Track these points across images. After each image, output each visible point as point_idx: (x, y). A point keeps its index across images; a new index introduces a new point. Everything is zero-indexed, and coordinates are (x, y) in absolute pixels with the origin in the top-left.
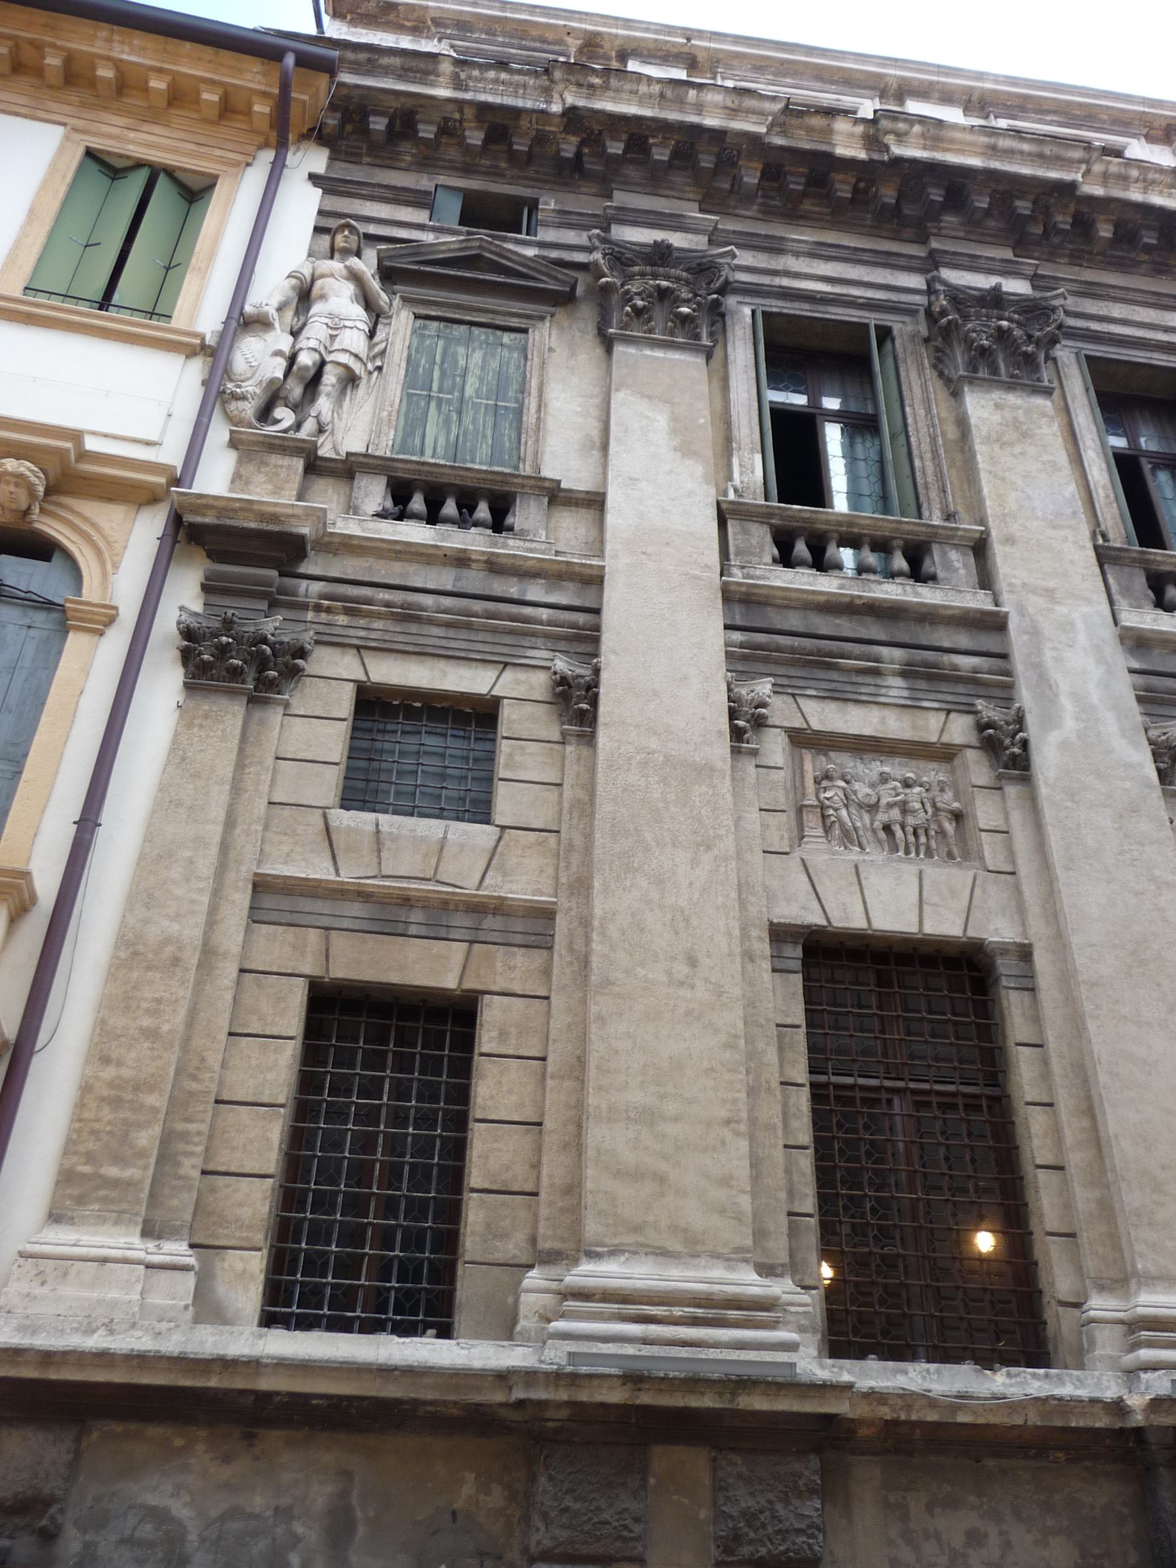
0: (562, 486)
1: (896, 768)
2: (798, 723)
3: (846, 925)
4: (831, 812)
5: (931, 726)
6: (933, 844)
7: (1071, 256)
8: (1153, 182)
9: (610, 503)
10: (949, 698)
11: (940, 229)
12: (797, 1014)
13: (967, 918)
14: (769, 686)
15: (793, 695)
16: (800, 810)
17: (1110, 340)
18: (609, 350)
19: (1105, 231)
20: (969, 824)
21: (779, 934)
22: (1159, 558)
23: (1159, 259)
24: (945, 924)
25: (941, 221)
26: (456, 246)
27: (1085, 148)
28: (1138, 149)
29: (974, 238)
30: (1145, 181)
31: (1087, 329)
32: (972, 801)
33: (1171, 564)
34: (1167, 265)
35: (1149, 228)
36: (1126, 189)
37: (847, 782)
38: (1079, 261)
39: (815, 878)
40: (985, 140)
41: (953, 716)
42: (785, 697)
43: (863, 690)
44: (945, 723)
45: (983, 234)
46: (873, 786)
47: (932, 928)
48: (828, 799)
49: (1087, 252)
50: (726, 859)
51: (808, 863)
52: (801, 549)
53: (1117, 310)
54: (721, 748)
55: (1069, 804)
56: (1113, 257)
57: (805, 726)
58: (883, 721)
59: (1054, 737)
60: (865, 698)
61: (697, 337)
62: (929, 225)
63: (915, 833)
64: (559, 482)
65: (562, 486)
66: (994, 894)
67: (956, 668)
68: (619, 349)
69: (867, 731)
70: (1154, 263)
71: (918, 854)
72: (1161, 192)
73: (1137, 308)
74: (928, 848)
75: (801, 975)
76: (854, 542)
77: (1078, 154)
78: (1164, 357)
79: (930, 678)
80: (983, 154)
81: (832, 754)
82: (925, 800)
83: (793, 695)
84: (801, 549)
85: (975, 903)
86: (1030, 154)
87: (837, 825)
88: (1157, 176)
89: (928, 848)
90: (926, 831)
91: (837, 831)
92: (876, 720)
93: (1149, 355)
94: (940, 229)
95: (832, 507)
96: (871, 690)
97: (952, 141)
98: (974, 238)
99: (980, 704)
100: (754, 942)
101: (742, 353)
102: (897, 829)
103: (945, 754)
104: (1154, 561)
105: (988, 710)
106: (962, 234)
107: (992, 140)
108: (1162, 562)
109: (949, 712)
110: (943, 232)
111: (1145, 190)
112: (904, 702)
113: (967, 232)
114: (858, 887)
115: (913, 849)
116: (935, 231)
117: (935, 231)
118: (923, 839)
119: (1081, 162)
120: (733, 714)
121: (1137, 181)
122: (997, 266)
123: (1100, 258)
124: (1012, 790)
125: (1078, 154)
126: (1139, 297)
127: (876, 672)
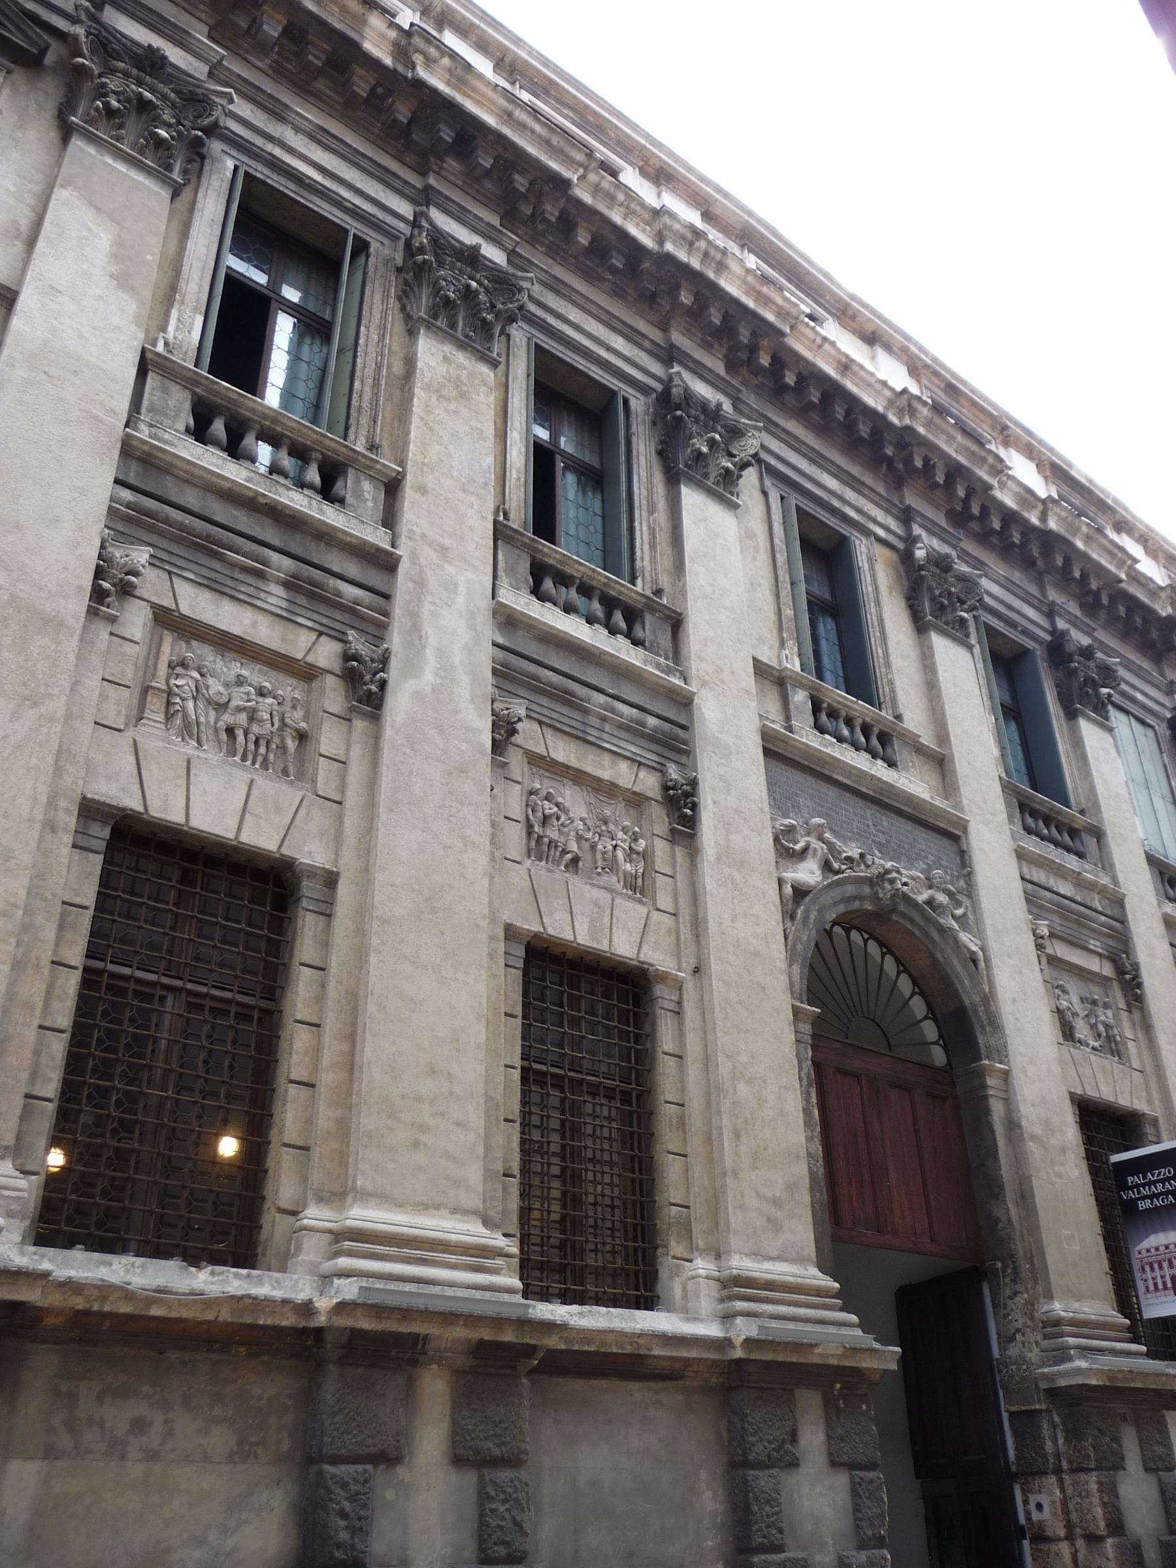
1: (255, 674)
2: (167, 602)
3: (163, 816)
4: (178, 700)
5: (300, 643)
6: (271, 757)
7: (549, 248)
8: (634, 212)
10: (325, 621)
13: (285, 836)
14: (146, 556)
15: (170, 573)
16: (146, 690)
20: (310, 746)
22: (546, 550)
24: (262, 836)
30: (627, 208)
31: (544, 321)
32: (319, 726)
37: (202, 675)
39: (142, 763)
41: (323, 639)
42: (161, 572)
43: (242, 589)
44: (314, 644)
45: (478, 191)
46: (227, 685)
47: (247, 838)
48: (177, 686)
50: (51, 720)
51: (140, 746)
54: (79, 604)
55: (408, 751)
57: (173, 607)
58: (254, 624)
59: (411, 685)
60: (242, 597)
62: (432, 159)
63: (257, 743)
66: (317, 818)
67: (339, 594)
69: (236, 630)
71: (254, 763)
72: (638, 224)
74: (266, 759)
79: (312, 596)
81: (194, 643)
82: (275, 713)
83: (170, 573)
85: (297, 822)
86: (539, 136)
87: (180, 715)
88: (638, 208)
89: (266, 759)
90: (268, 743)
91: (178, 721)
92: (247, 622)
94: (441, 168)
96: (251, 590)
99: (352, 635)
100: (61, 813)
102: (240, 734)
103: (306, 673)
104: (541, 551)
105: (358, 643)
106: (459, 183)
109: (321, 634)
110: (443, 173)
112: (279, 612)
113: (465, 183)
114: (185, 782)
115: (250, 757)
117: (436, 168)
118: (262, 750)
119: (581, 165)
120: (99, 573)
124: (359, 724)
126: (594, 309)
127: (260, 575)
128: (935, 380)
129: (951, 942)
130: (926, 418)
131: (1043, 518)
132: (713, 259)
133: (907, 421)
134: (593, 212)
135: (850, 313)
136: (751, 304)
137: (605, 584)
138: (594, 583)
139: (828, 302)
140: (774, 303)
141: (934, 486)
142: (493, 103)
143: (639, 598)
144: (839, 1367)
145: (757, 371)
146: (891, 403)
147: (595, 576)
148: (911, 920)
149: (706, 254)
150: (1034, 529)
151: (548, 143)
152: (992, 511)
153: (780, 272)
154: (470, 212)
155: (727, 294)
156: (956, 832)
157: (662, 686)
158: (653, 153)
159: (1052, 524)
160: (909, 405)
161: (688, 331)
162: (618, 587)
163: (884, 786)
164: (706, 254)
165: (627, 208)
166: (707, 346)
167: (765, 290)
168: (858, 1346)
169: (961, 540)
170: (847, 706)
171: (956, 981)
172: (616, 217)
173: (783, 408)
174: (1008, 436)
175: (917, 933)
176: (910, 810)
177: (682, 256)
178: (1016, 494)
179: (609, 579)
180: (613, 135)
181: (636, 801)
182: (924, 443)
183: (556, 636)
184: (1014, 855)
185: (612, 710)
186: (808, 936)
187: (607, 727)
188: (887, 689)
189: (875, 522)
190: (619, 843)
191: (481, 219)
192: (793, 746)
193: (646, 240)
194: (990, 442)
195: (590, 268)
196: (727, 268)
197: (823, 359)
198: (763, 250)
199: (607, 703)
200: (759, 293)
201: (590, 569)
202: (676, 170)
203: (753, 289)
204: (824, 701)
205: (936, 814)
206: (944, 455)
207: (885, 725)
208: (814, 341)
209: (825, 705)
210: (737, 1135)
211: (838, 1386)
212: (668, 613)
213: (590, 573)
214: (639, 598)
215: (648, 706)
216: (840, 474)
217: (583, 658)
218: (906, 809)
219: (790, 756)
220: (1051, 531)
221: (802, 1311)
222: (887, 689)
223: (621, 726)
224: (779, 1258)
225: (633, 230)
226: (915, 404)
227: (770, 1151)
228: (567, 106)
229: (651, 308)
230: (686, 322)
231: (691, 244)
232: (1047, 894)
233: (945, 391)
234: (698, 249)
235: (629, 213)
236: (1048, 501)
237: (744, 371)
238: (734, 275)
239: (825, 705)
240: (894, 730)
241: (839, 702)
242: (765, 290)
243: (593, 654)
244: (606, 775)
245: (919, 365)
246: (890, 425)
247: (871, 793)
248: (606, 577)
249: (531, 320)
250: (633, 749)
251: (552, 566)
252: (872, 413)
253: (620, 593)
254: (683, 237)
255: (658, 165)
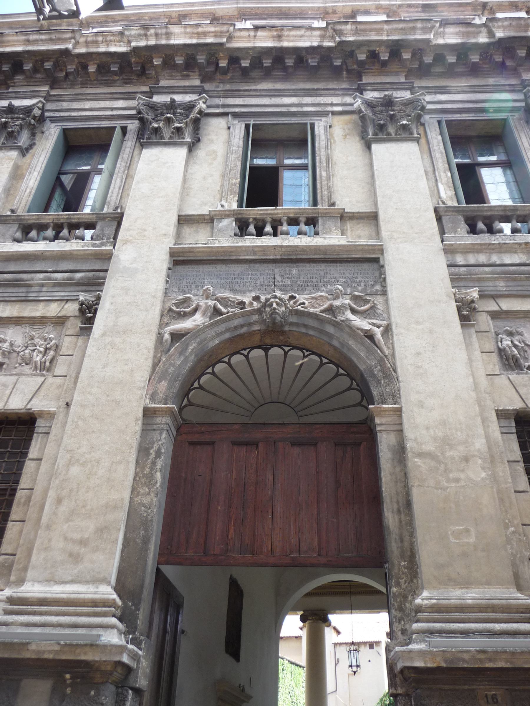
0: (346, 211)
7: (81, 84)
8: (111, 41)
9: (382, 215)
11: (14, 83)
12: (517, 454)
17: (81, 119)
18: (369, 147)
19: (92, 69)
21: (501, 414)
22: (26, 217)
23: (125, 77)
25: (14, 79)
26: (510, 105)
27: (71, 32)
28: (266, 17)
29: (32, 84)
30: (106, 41)
31: (70, 116)
33: (33, 219)
34: (130, 79)
35: (115, 63)
36: (98, 47)
38: (86, 86)
40: (23, 38)
45: (35, 82)
49: (89, 81)
52: (481, 225)
53: (287, 100)
56: (102, 80)
61: (412, 134)
62: (9, 82)
64: (344, 209)
65: (346, 211)
68: (375, 147)
70: (122, 79)
72: (115, 45)
73: (100, 102)
75: (515, 435)
76: (506, 219)
77: (69, 35)
78: (108, 122)
80: (24, 44)
84: (481, 225)
86: (46, 40)
88: (112, 38)
93: (100, 123)
94: (14, 83)
95: (490, 203)
97: (8, 41)
98: (32, 84)
101: (436, 139)
104: (24, 219)
106: (25, 83)
107: (26, 37)
108: (28, 219)
110: (16, 84)
111: (108, 46)
113: (27, 82)
116: (12, 84)
117: (12, 84)
119: (71, 38)
121: (102, 42)
122: (28, 94)
123: (96, 82)
125: (69, 35)
126: (102, 96)
128: (412, 10)
129: (347, 329)
130: (352, 30)
131: (491, 34)
132: (162, 34)
133: (338, 39)
134: (90, 54)
135: (330, 11)
136: (194, 41)
137: (68, 219)
138: (62, 221)
139: (311, 14)
140: (209, 32)
141: (384, 64)
142: (18, 41)
143: (91, 216)
144: (53, 660)
145: (224, 72)
146: (323, 37)
147: (60, 217)
148: (305, 326)
149: (157, 35)
150: (489, 45)
151: (51, 40)
152: (445, 53)
153: (272, 18)
154: (19, 92)
155: (178, 45)
156: (374, 256)
157: (88, 254)
158: (170, 11)
159: (500, 34)
160: (335, 30)
161: (171, 76)
162: (76, 216)
163: (288, 249)
164: (157, 35)
165: (106, 41)
166: (187, 77)
167: (200, 30)
168: (74, 643)
169: (413, 82)
170: (270, 214)
171: (349, 354)
172: (102, 49)
173: (255, 80)
174: (491, 8)
175: (311, 332)
176: (321, 256)
177: (143, 43)
178: (457, 33)
179: (69, 214)
180: (147, 18)
181: (60, 321)
182: (360, 44)
183: (13, 255)
184: (442, 252)
185: (49, 279)
186: (181, 362)
187: (44, 289)
188: (326, 193)
189: (332, 105)
190: (38, 347)
191: (26, 92)
192: (199, 252)
193: (122, 49)
194: (474, 19)
195: (107, 80)
196: (172, 33)
197: (261, 41)
198: (256, 14)
199: (45, 277)
200: (198, 33)
201: (55, 215)
202: (185, 11)
203: (193, 33)
204: (249, 219)
205: (347, 251)
206: (380, 43)
207: (308, 213)
208: (249, 36)
209: (251, 220)
210: (59, 501)
211: (68, 676)
212: (112, 216)
213: (56, 217)
214: (91, 216)
215: (78, 269)
216: (295, 93)
217: (34, 260)
218: (316, 257)
219: (199, 258)
220: (501, 40)
221: (498, 627)
222: (326, 193)
223: (55, 285)
224: (72, 582)
225: (113, 49)
226: (338, 27)
227: (89, 507)
228: (119, 21)
229: (147, 78)
230: (167, 73)
231: (146, 35)
232: (487, 269)
233: (423, 11)
234: (151, 35)
235: (108, 43)
236: (487, 23)
237: (218, 76)
238: (178, 34)
239: (251, 220)
240: (318, 213)
241: (261, 214)
242: (200, 30)
243: (38, 255)
244: (37, 314)
245: (395, 8)
246: (329, 48)
247: (278, 257)
248: (67, 214)
249: (53, 120)
250: (63, 294)
251: (34, 223)
252: (311, 50)
253: (78, 219)
254: (139, 35)
255: (177, 14)
